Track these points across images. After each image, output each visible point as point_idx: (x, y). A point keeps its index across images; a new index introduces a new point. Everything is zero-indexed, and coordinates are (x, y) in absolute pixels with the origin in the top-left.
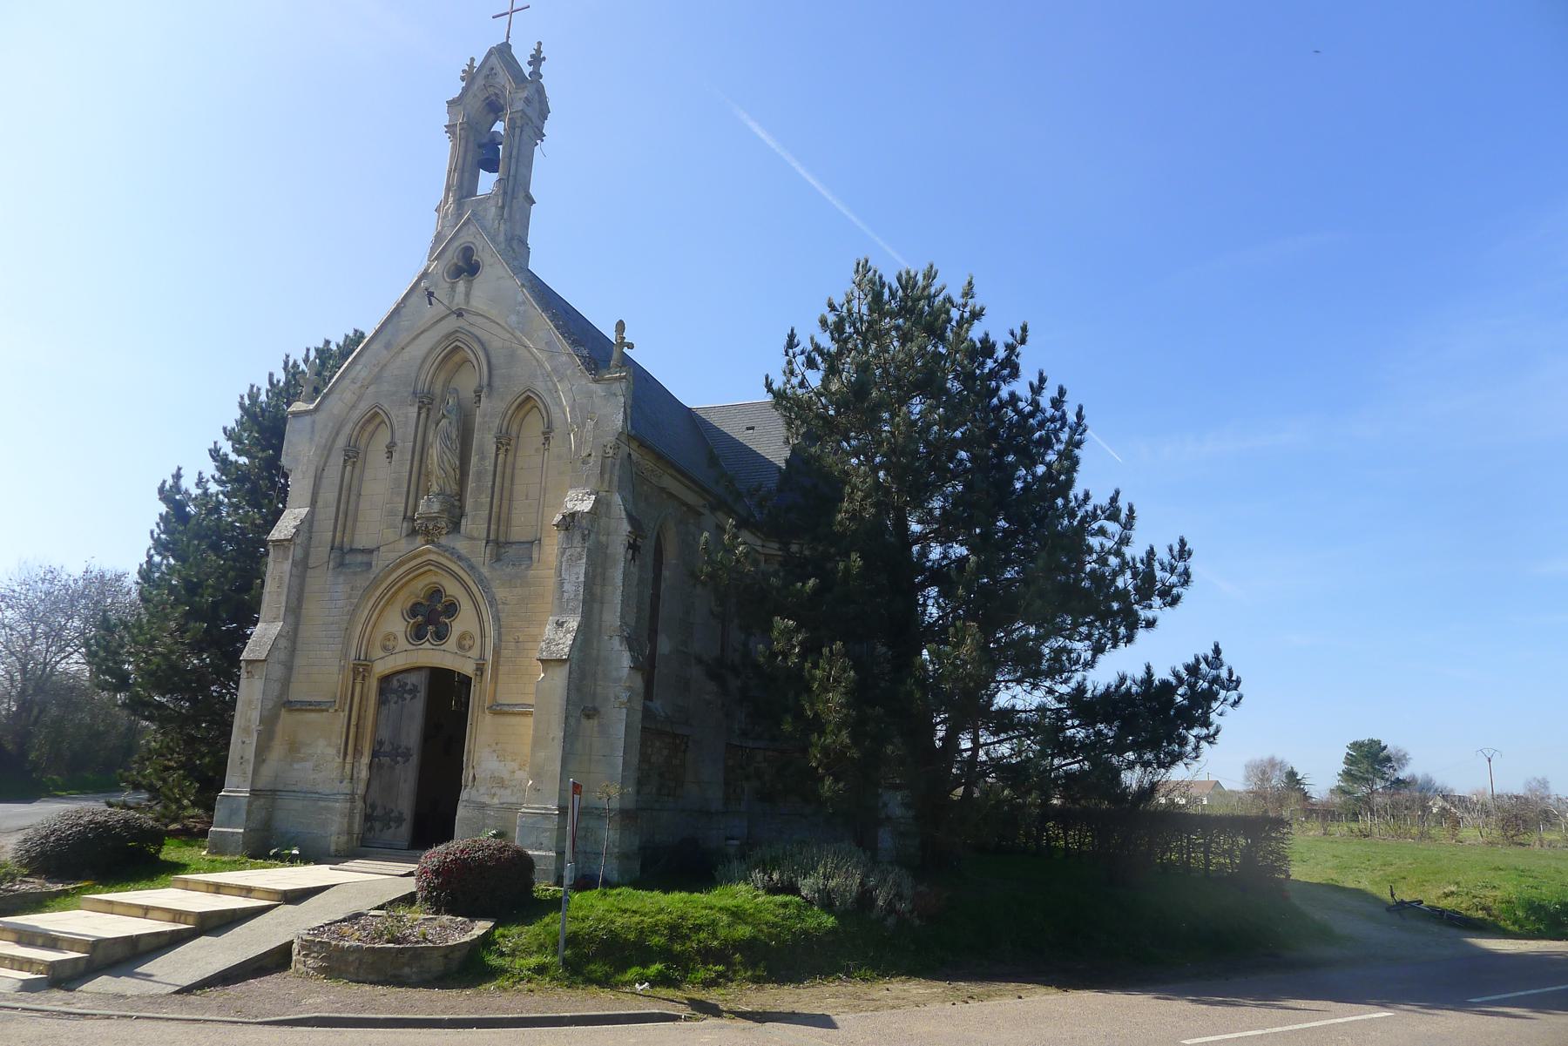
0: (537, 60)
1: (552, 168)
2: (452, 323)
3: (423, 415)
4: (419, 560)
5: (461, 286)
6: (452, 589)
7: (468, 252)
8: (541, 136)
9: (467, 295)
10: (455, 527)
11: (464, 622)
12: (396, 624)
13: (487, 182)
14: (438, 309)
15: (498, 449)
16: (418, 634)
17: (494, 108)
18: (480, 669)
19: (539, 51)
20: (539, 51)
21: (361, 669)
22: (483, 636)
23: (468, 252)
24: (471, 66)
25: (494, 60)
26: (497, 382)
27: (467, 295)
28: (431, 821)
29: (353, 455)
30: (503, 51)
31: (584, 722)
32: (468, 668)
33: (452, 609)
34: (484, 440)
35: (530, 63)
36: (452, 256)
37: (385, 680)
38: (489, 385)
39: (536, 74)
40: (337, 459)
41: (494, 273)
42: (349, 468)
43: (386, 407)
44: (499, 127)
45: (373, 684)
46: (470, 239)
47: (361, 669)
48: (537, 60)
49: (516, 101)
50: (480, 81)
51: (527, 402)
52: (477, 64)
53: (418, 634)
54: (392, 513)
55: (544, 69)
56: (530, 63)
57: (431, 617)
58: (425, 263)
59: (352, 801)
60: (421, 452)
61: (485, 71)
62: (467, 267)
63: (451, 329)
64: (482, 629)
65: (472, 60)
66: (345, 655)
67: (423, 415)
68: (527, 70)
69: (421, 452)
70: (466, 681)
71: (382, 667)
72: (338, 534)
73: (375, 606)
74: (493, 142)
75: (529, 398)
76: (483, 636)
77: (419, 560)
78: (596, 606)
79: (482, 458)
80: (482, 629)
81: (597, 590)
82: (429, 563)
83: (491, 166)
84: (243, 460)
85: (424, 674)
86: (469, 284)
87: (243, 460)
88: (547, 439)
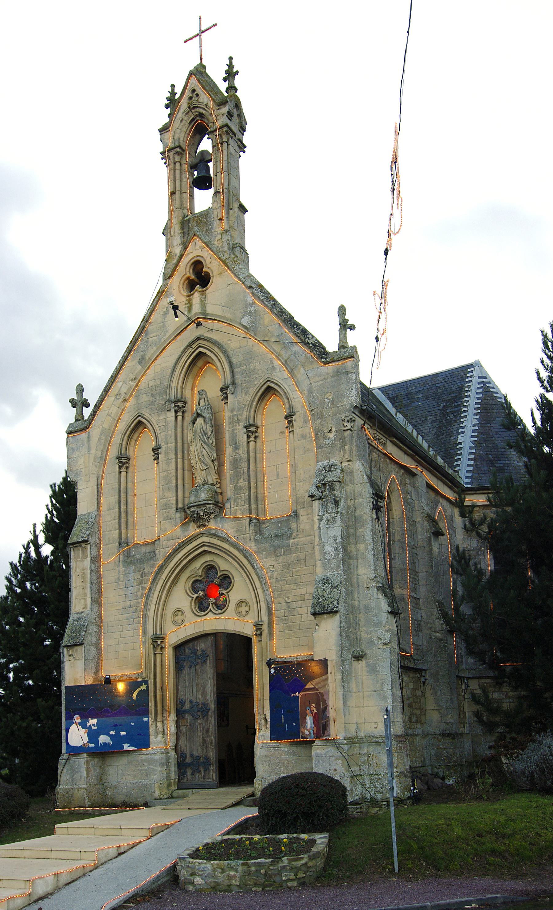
0: (231, 74)
1: (257, 172)
2: (192, 333)
3: (180, 418)
4: (195, 544)
5: (196, 297)
6: (223, 565)
7: (197, 265)
8: (242, 147)
9: (203, 304)
10: (220, 506)
11: (238, 592)
12: (182, 598)
13: (203, 200)
14: (181, 319)
15: (248, 437)
16: (202, 606)
17: (200, 130)
18: (258, 627)
19: (231, 66)
20: (231, 66)
21: (157, 641)
22: (258, 602)
23: (197, 265)
24: (173, 93)
25: (193, 80)
26: (239, 379)
27: (203, 304)
28: (235, 766)
29: (124, 461)
30: (199, 72)
31: (355, 663)
32: (248, 630)
33: (226, 581)
34: (234, 431)
35: (225, 80)
36: (184, 270)
37: (179, 648)
38: (234, 383)
39: (232, 88)
40: (112, 466)
41: (221, 284)
42: (123, 474)
43: (147, 415)
44: (206, 145)
45: (169, 654)
46: (198, 253)
47: (157, 641)
48: (231, 74)
49: (218, 118)
50: (184, 104)
51: (269, 391)
52: (178, 90)
53: (202, 606)
54: (165, 507)
55: (238, 82)
56: (225, 80)
57: (210, 589)
58: (161, 283)
59: (167, 765)
60: (183, 450)
61: (188, 93)
62: (200, 279)
63: (193, 338)
64: (257, 596)
65: (173, 86)
66: (145, 632)
67: (180, 418)
68: (223, 86)
69: (183, 450)
70: (248, 641)
71: (175, 635)
72: (123, 531)
73: (162, 591)
74: (203, 160)
75: (269, 388)
76: (258, 602)
77: (195, 544)
78: (353, 562)
79: (236, 448)
80: (257, 596)
81: (352, 548)
82: (205, 552)
83: (204, 182)
84: (49, 562)
85: (210, 640)
86: (203, 293)
87: (49, 562)
88: (290, 422)
